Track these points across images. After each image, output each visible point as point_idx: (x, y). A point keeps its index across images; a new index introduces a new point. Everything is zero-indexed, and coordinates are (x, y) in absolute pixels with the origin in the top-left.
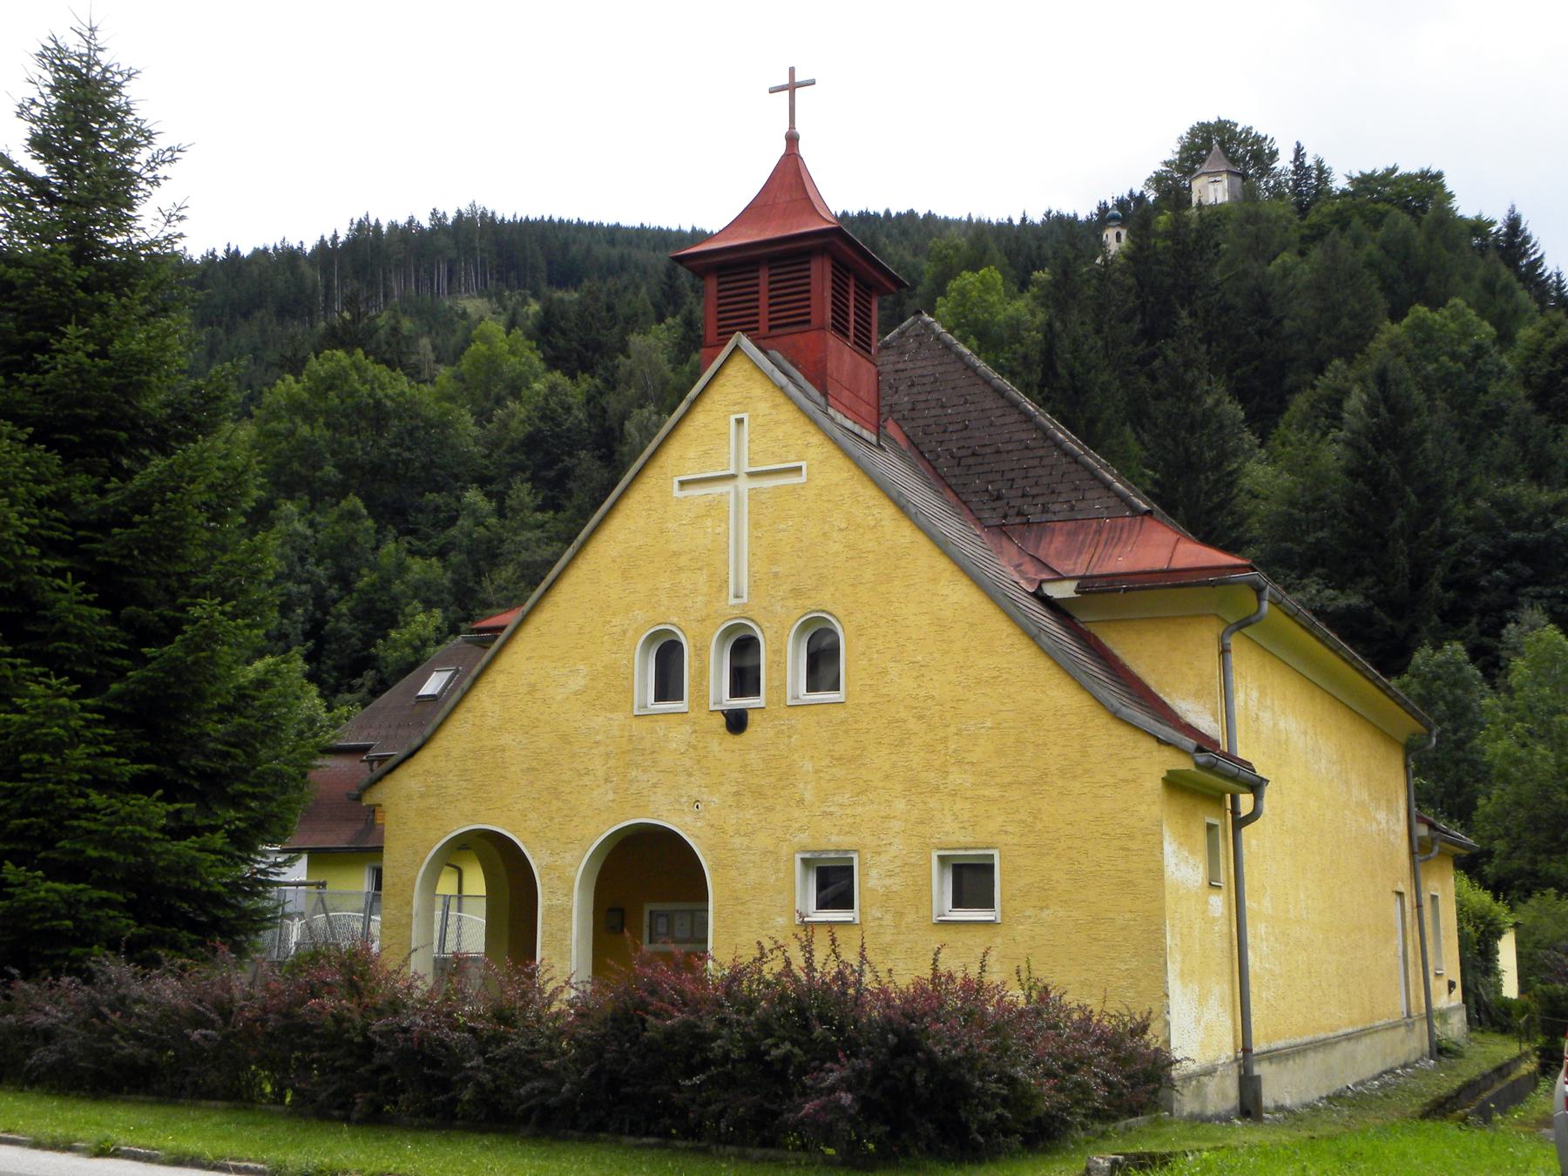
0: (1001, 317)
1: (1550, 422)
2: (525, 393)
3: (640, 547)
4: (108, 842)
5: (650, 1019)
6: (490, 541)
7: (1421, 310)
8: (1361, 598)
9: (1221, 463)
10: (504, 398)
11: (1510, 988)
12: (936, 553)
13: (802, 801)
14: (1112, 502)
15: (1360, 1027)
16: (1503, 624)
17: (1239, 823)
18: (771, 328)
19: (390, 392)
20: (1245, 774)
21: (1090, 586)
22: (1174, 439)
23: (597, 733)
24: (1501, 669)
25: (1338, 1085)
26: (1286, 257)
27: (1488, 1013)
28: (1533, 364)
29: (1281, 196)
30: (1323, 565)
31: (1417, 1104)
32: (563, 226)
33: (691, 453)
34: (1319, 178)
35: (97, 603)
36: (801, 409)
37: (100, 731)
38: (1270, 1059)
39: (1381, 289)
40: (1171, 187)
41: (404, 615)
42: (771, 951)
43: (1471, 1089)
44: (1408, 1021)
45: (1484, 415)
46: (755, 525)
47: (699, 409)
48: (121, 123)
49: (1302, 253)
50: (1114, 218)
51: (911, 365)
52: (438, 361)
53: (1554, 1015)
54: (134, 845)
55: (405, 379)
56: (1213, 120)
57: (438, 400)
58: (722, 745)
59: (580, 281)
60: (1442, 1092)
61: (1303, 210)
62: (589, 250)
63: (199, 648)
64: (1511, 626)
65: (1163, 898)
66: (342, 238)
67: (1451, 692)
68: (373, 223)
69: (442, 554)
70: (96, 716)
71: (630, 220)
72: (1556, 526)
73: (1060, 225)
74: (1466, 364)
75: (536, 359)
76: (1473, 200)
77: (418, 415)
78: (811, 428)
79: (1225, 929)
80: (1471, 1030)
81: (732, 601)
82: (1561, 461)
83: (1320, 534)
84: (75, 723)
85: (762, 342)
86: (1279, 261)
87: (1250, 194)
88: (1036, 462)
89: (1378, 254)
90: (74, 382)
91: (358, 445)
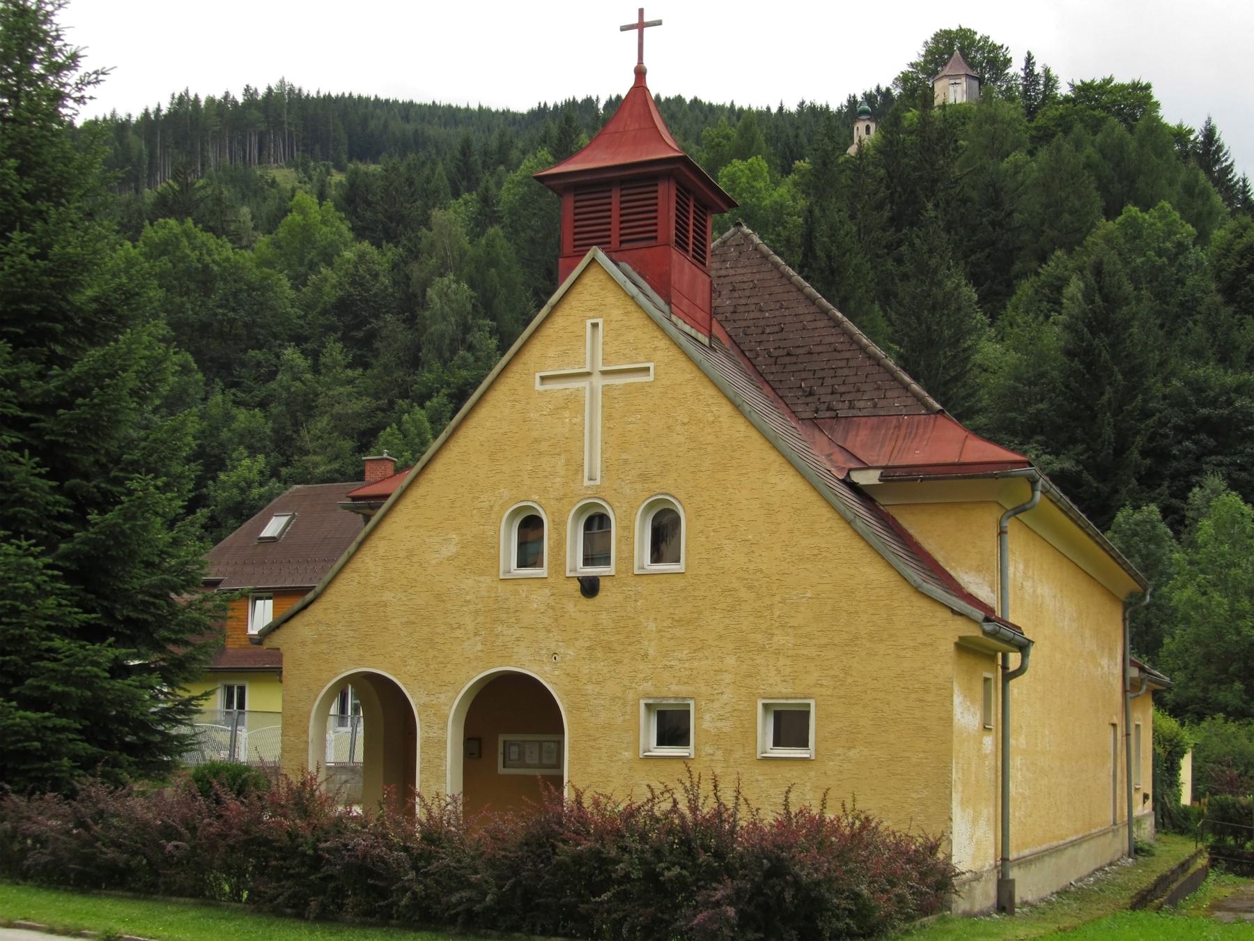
0: (767, 202)
1: (1235, 313)
2: (336, 259)
3: (505, 433)
4: (66, 679)
5: (561, 845)
6: (306, 395)
7: (1132, 210)
8: (1073, 463)
9: (958, 341)
10: (317, 264)
11: (1186, 799)
12: (766, 446)
13: (646, 655)
14: (910, 401)
15: (1080, 835)
16: (1189, 487)
17: (1008, 676)
18: (621, 242)
19: (216, 257)
20: (1009, 633)
21: (890, 475)
22: (918, 318)
23: (467, 593)
24: (1186, 526)
25: (1064, 882)
26: (1019, 156)
27: (1170, 817)
28: (1223, 261)
29: (1011, 99)
30: (1042, 433)
31: (1125, 898)
32: (362, 102)
33: (552, 352)
34: (1046, 85)
35: (47, 477)
36: (650, 317)
37: (59, 585)
38: (1019, 865)
39: (1097, 189)
40: (916, 87)
41: (232, 460)
42: (662, 793)
43: (1163, 881)
44: (1114, 828)
45: (1182, 304)
46: (607, 417)
47: (559, 313)
48: (51, 47)
49: (1031, 153)
50: (864, 112)
51: (732, 272)
52: (255, 228)
53: (1224, 819)
54: (87, 682)
55: (229, 245)
56: (954, 28)
57: (258, 266)
58: (578, 607)
59: (379, 153)
60: (1144, 886)
61: (1031, 112)
62: (386, 126)
63: (134, 517)
64: (1196, 490)
65: (951, 741)
66: (164, 111)
67: (1146, 547)
68: (192, 96)
69: (263, 405)
70: (56, 572)
71: (423, 97)
72: (1237, 404)
73: (813, 115)
74: (1169, 259)
75: (344, 228)
76: (1178, 110)
77: (241, 279)
78: (658, 334)
79: (993, 763)
80: (1157, 832)
81: (587, 483)
82: (1243, 347)
83: (1041, 406)
84: (39, 579)
85: (614, 255)
86: (1011, 158)
87: (987, 98)
88: (843, 363)
89: (1096, 157)
90: (19, 280)
91: (189, 306)
